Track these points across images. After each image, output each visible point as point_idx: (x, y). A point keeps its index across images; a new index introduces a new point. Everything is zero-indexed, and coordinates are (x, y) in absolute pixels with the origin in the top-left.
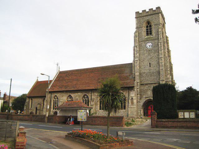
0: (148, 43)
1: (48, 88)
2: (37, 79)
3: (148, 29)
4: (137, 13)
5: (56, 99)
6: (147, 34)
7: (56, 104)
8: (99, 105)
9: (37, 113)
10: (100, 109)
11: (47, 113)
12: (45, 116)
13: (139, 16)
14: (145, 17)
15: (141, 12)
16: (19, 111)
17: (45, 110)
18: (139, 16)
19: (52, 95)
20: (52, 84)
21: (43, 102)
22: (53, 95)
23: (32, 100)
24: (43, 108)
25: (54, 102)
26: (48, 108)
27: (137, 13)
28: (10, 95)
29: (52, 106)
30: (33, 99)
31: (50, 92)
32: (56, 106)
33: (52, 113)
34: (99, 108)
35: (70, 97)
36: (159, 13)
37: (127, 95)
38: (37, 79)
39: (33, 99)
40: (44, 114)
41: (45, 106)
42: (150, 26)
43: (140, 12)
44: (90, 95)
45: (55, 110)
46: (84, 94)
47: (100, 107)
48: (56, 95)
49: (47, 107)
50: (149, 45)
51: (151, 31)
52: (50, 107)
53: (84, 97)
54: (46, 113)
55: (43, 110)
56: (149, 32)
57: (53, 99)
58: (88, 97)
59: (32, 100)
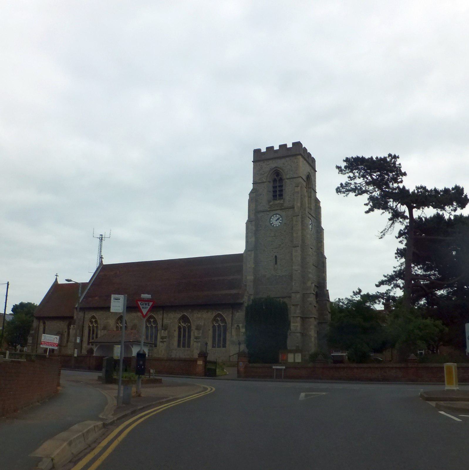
0: (275, 216)
1: (79, 301)
2: (56, 279)
3: (276, 187)
4: (257, 152)
5: (220, 323)
6: (273, 196)
7: (93, 333)
8: (176, 339)
9: (83, 351)
10: (179, 346)
11: (76, 350)
12: (72, 356)
13: (259, 157)
14: (270, 162)
15: (264, 150)
16: (19, 347)
17: (71, 345)
18: (259, 157)
19: (86, 316)
20: (87, 293)
21: (66, 330)
22: (89, 315)
23: (44, 323)
24: (67, 341)
25: (90, 330)
26: (78, 341)
27: (257, 152)
28: (6, 313)
29: (85, 339)
30: (47, 323)
31: (83, 309)
32: (93, 339)
33: (84, 352)
34: (176, 343)
35: (185, 319)
36: (298, 155)
37: (230, 320)
38: (56, 279)
39: (47, 323)
40: (69, 352)
41: (72, 338)
42: (281, 180)
43: (275, 149)
44: (161, 317)
45: (90, 346)
46: (215, 313)
47: (179, 341)
48: (221, 313)
49: (76, 340)
50: (275, 221)
51: (281, 191)
52: (82, 341)
53: (215, 319)
54: (74, 350)
55: (66, 346)
56: (278, 192)
57: (87, 324)
58: (223, 320)
59: (44, 323)
